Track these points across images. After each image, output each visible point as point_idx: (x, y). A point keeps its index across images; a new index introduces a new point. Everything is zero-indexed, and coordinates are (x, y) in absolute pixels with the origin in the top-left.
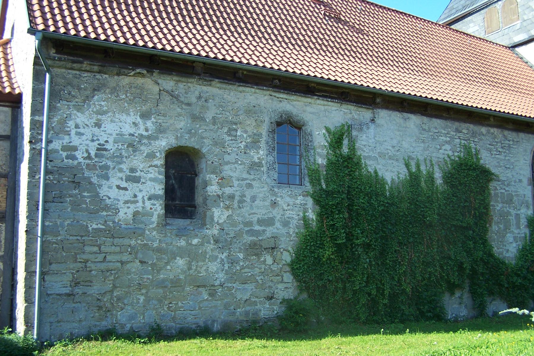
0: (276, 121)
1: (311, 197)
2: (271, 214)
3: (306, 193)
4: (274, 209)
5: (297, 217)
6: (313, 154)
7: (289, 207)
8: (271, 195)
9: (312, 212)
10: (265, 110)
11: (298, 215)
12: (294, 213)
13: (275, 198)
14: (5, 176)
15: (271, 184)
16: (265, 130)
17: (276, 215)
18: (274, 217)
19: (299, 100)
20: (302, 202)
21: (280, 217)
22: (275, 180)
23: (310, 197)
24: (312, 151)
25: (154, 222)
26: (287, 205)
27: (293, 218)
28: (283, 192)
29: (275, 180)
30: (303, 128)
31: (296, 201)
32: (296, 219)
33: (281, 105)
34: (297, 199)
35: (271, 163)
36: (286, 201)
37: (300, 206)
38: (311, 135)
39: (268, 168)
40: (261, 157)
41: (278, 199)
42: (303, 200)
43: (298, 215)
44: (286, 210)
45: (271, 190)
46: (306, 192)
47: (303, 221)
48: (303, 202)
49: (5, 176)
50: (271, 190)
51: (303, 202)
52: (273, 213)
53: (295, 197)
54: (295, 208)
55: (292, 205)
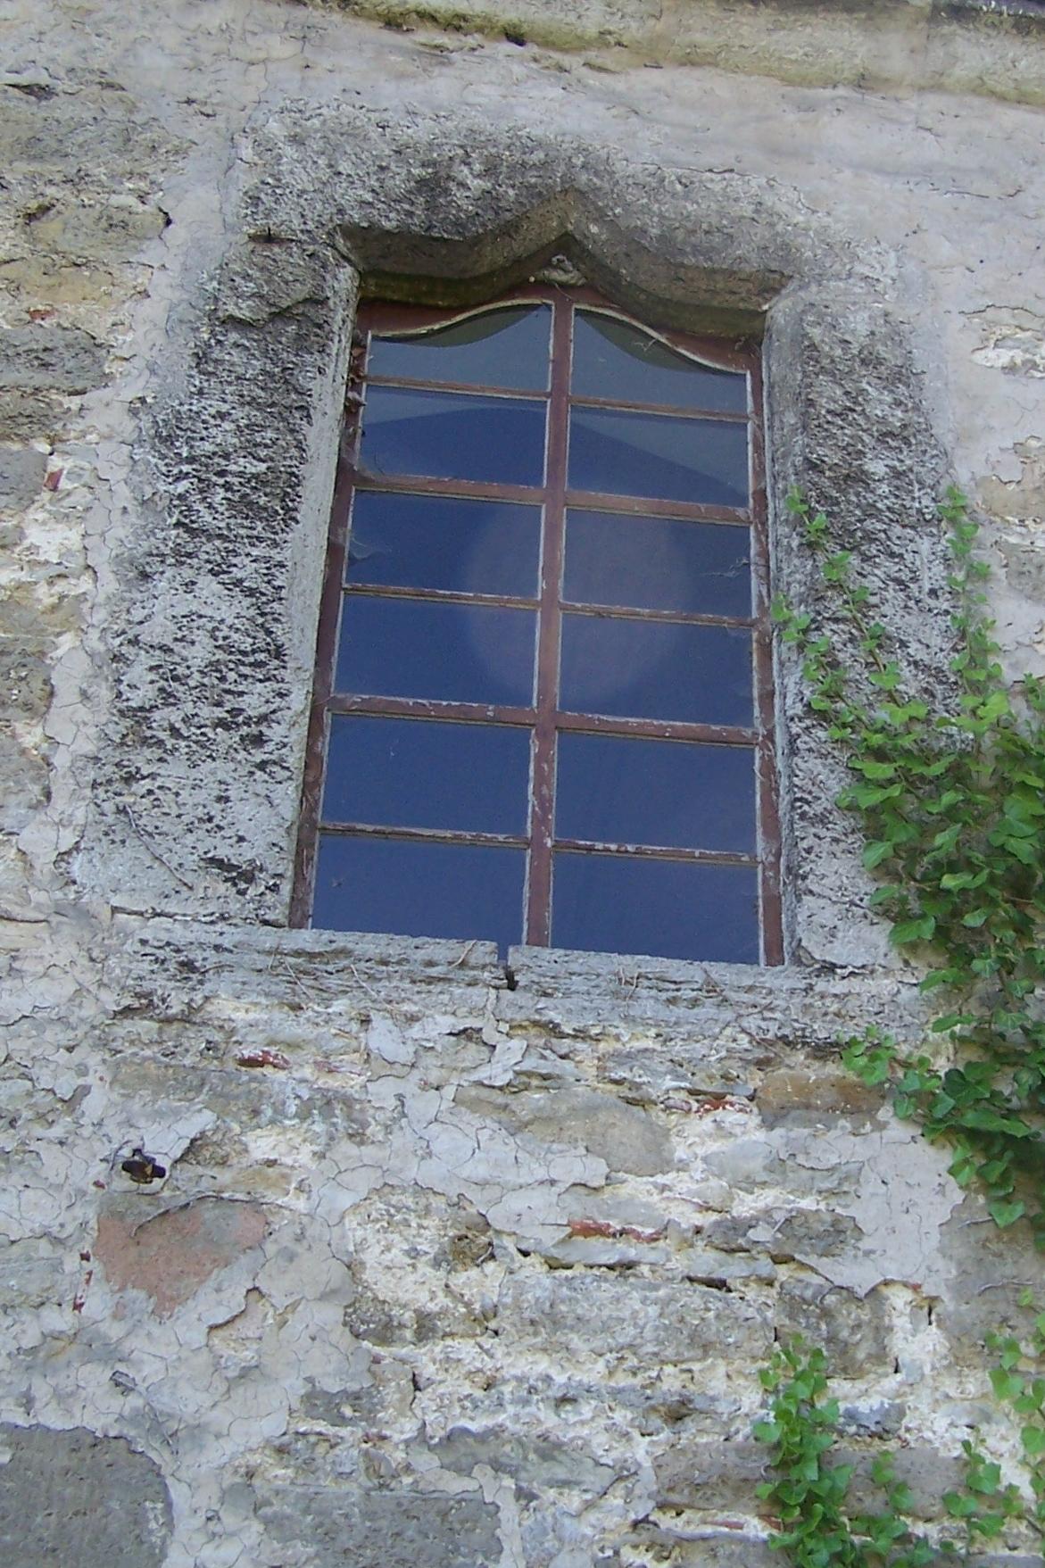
0: (350, 232)
1: (939, 1128)
2: (95, 1377)
3: (833, 1069)
4: (166, 1304)
5: (641, 1450)
6: (934, 574)
7: (483, 1283)
8: (126, 1078)
9: (956, 1362)
10: (197, 129)
11: (678, 1413)
12: (593, 1372)
13: (201, 1120)
14: (1005, 1567)
15: (155, 930)
16: (152, 310)
17: (189, 1400)
18: (154, 1421)
19: (704, 39)
20: (746, 1205)
21: (272, 1426)
22: (240, 876)
23: (899, 1131)
24: (925, 552)
25: (996, 1550)
26: (431, 1237)
27: (549, 1449)
28: (382, 1037)
29: (240, 876)
30: (780, 310)
31: (636, 1188)
32: (624, 1474)
33: (442, 86)
34: (658, 1161)
35: (200, 653)
36: (428, 1173)
37: (706, 1260)
38: (901, 376)
39: (140, 715)
40: (45, 595)
41: (262, 1144)
42: (778, 1167)
43: (678, 1413)
44: (426, 1328)
45: (143, 1005)
46: (825, 1051)
47: (775, 1506)
48: (767, 1198)
49: (1005, 1567)
50: (143, 1005)
51: (767, 1198)
52: (148, 1371)
53: (627, 1130)
54: (609, 1288)
55: (549, 1238)
